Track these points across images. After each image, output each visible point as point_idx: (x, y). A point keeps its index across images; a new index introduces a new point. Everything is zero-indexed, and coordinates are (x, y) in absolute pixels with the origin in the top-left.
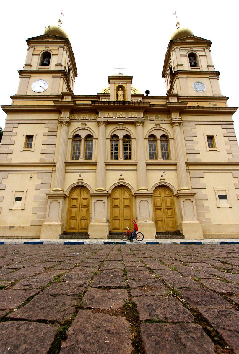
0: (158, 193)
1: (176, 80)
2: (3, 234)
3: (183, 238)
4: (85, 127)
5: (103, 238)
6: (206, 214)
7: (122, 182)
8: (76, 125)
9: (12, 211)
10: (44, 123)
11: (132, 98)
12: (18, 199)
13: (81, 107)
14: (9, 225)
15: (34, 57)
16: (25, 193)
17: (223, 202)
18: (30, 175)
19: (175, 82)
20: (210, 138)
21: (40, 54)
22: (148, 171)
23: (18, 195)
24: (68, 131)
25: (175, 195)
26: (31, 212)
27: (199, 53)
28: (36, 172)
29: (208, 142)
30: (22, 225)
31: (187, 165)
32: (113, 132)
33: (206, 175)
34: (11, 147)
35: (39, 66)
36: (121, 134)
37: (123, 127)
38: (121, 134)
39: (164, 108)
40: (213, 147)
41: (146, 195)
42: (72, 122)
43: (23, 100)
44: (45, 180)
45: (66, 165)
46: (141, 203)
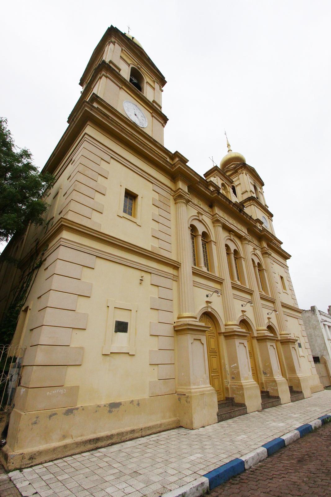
1: (101, 78)
2: (95, 433)
5: (183, 426)
9: (108, 358)
10: (152, 183)
12: (121, 327)
13: (201, 188)
14: (104, 401)
18: (138, 274)
19: (99, 81)
20: (130, 196)
22: (195, 285)
25: (223, 333)
26: (149, 364)
28: (149, 271)
29: (125, 201)
30: (136, 398)
39: (209, 194)
40: (131, 215)
44: (165, 293)
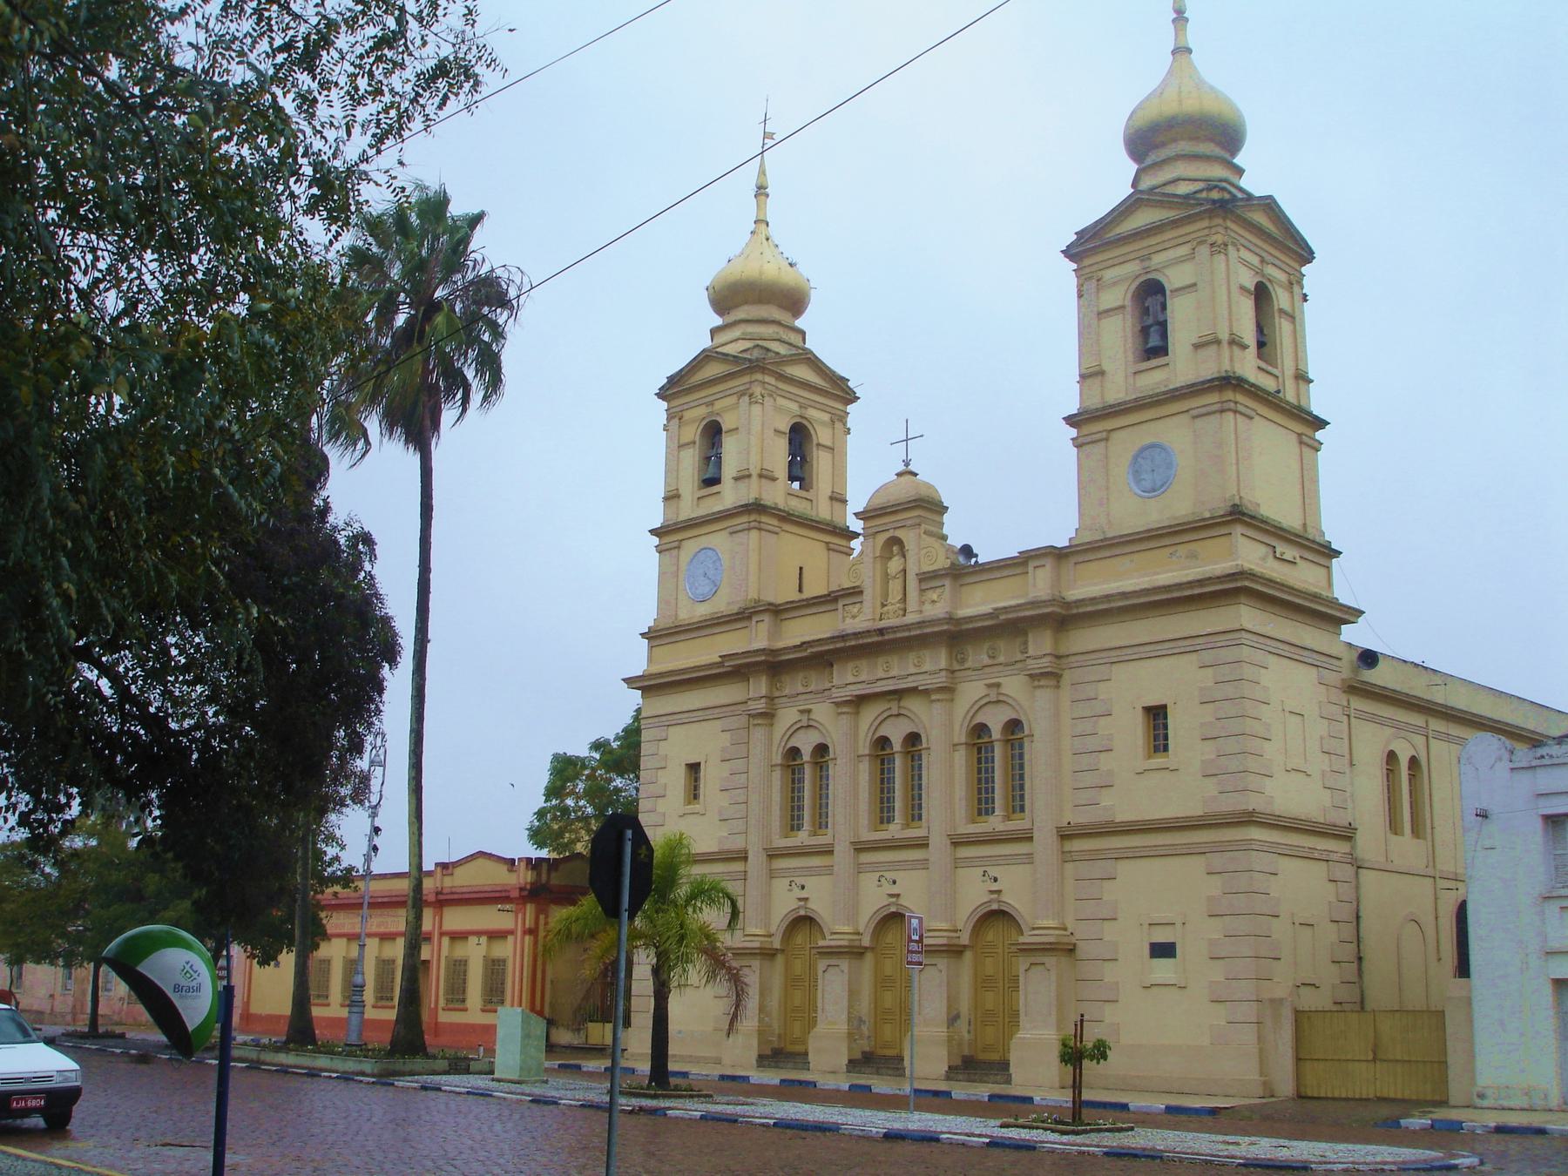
0: (990, 936)
3: (1008, 1081)
4: (809, 719)
6: (1108, 1007)
7: (893, 903)
8: (972, 691)
11: (923, 587)
12: (1163, 950)
15: (683, 454)
16: (1179, 926)
17: (1163, 969)
21: (1128, 302)
23: (1161, 936)
24: (857, 727)
27: (1173, 278)
31: (1066, 835)
32: (876, 729)
33: (1125, 869)
34: (1105, 762)
35: (700, 489)
36: (896, 733)
37: (899, 707)
38: (896, 733)
41: (742, 954)
42: (779, 706)
43: (673, 640)
45: (771, 857)
46: (1030, 973)
